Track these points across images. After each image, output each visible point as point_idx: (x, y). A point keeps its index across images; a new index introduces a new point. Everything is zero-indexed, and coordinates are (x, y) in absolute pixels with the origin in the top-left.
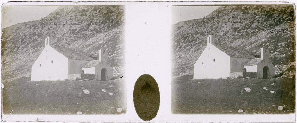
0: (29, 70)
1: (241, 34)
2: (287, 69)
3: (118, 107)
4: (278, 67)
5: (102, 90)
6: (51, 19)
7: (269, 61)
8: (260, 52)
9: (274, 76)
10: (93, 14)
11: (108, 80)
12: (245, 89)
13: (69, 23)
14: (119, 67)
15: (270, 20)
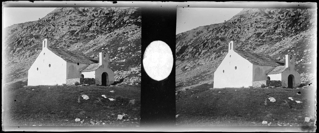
0: (211, 77)
1: (78, 38)
2: (127, 75)
3: (306, 116)
4: (118, 73)
5: (103, 96)
6: (235, 22)
7: (108, 66)
8: (285, 59)
9: (113, 82)
10: (279, 17)
11: (109, 85)
12: (82, 96)
13: (68, 24)
14: (307, 74)
15: (296, 25)
